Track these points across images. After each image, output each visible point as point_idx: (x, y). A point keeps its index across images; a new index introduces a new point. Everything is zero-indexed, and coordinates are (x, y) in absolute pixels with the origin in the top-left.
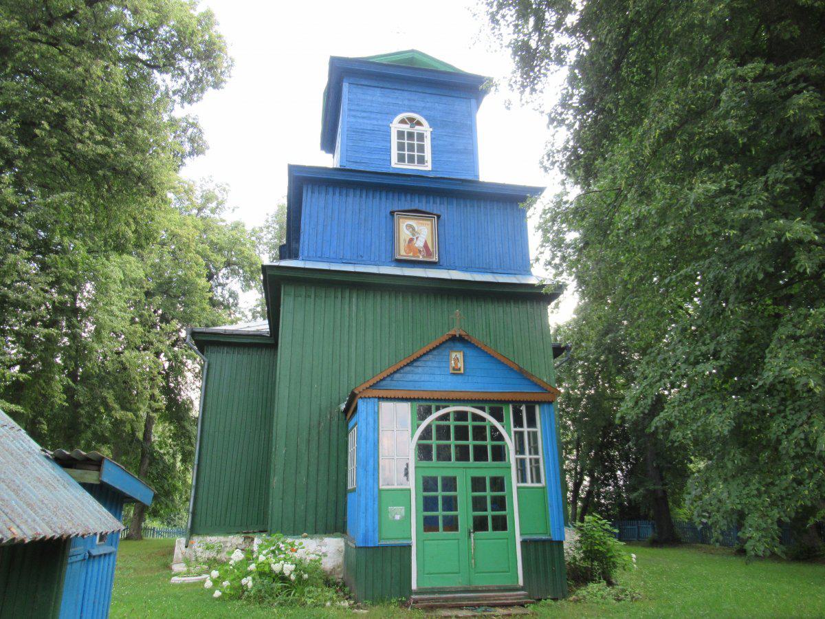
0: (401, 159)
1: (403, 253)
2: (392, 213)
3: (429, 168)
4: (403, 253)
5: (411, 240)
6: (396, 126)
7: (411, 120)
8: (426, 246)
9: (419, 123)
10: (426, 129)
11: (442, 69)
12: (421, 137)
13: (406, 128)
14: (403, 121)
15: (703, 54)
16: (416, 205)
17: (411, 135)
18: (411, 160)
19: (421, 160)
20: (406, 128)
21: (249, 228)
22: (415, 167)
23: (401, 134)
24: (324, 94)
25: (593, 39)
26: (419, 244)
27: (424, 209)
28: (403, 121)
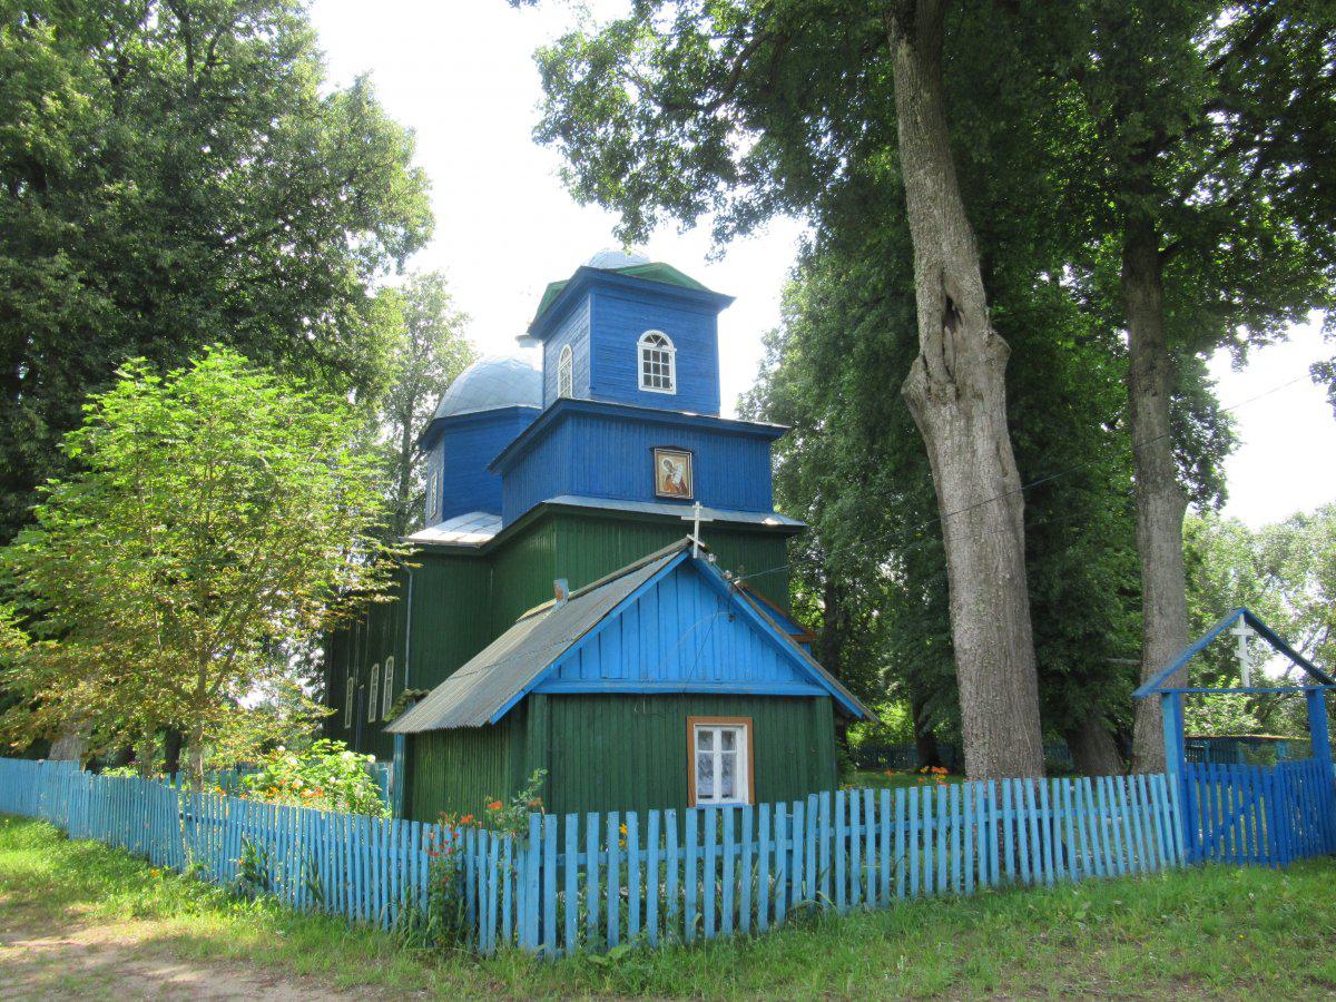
0: (647, 381)
1: (662, 489)
2: (652, 450)
3: (673, 391)
4: (662, 490)
5: (669, 477)
6: (642, 345)
7: (657, 338)
8: (682, 483)
9: (663, 342)
10: (670, 349)
11: (689, 285)
12: (666, 357)
13: (652, 347)
14: (648, 340)
15: (351, 307)
16: (677, 442)
17: (656, 355)
18: (657, 385)
19: (667, 384)
20: (652, 347)
21: (316, 46)
22: (661, 390)
23: (647, 353)
24: (671, 268)
25: (1045, 277)
26: (676, 480)
27: (683, 446)
28: (648, 340)
